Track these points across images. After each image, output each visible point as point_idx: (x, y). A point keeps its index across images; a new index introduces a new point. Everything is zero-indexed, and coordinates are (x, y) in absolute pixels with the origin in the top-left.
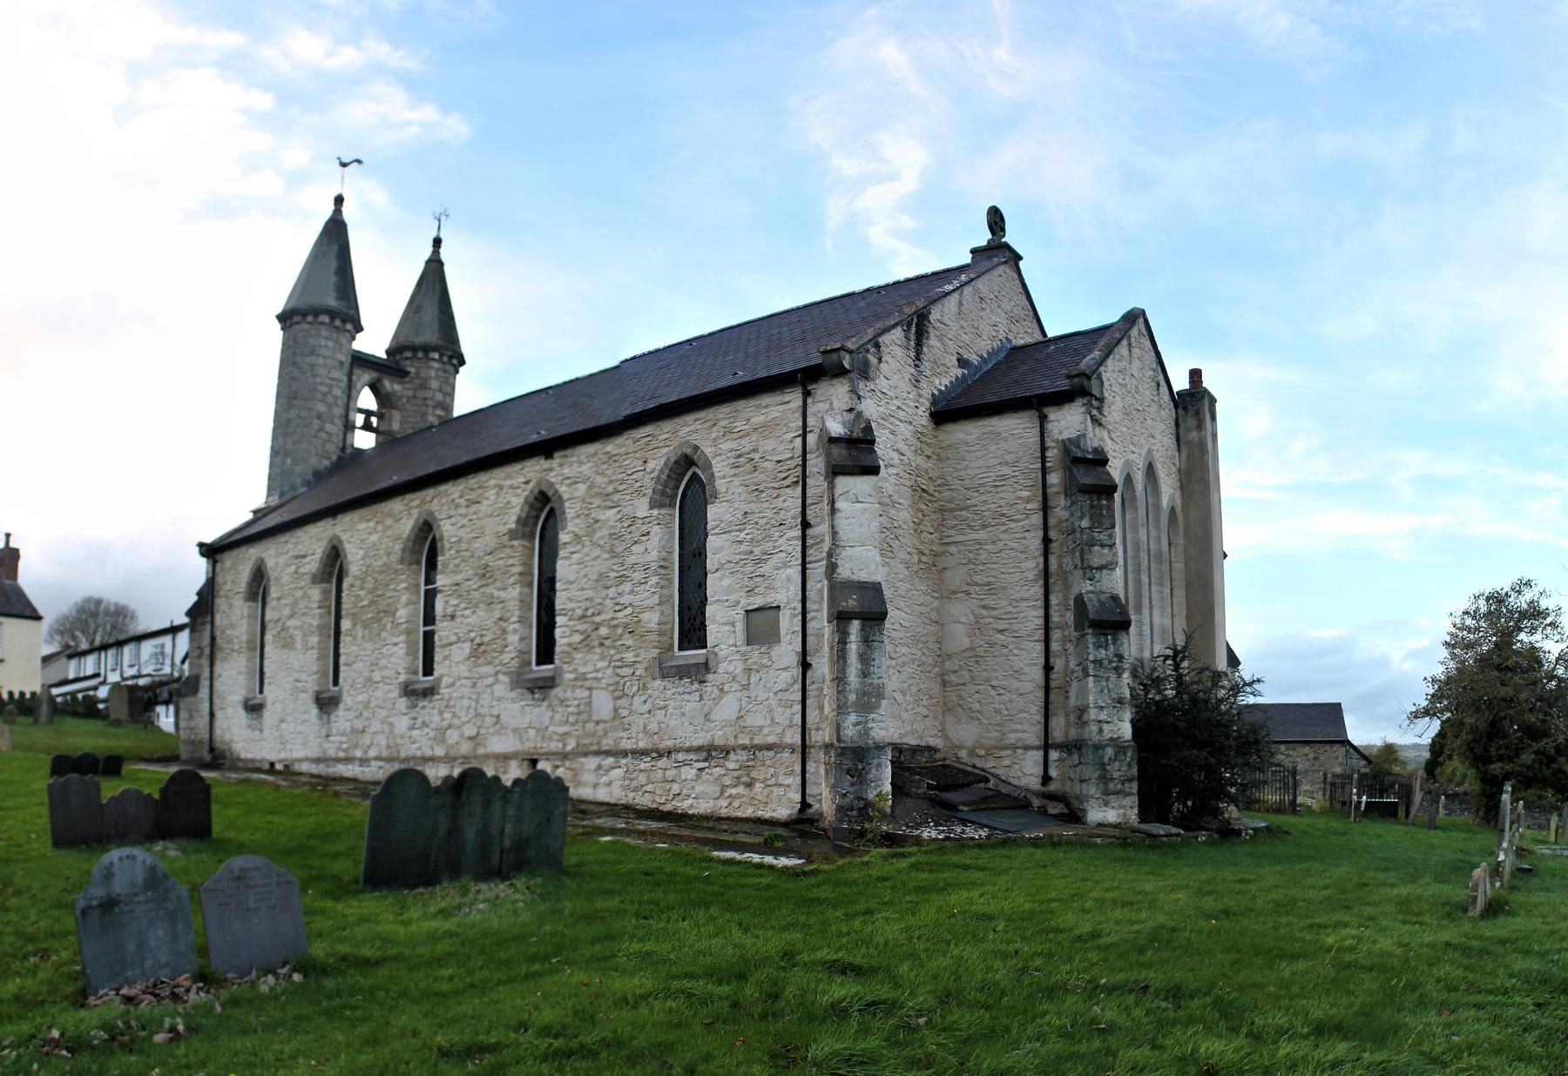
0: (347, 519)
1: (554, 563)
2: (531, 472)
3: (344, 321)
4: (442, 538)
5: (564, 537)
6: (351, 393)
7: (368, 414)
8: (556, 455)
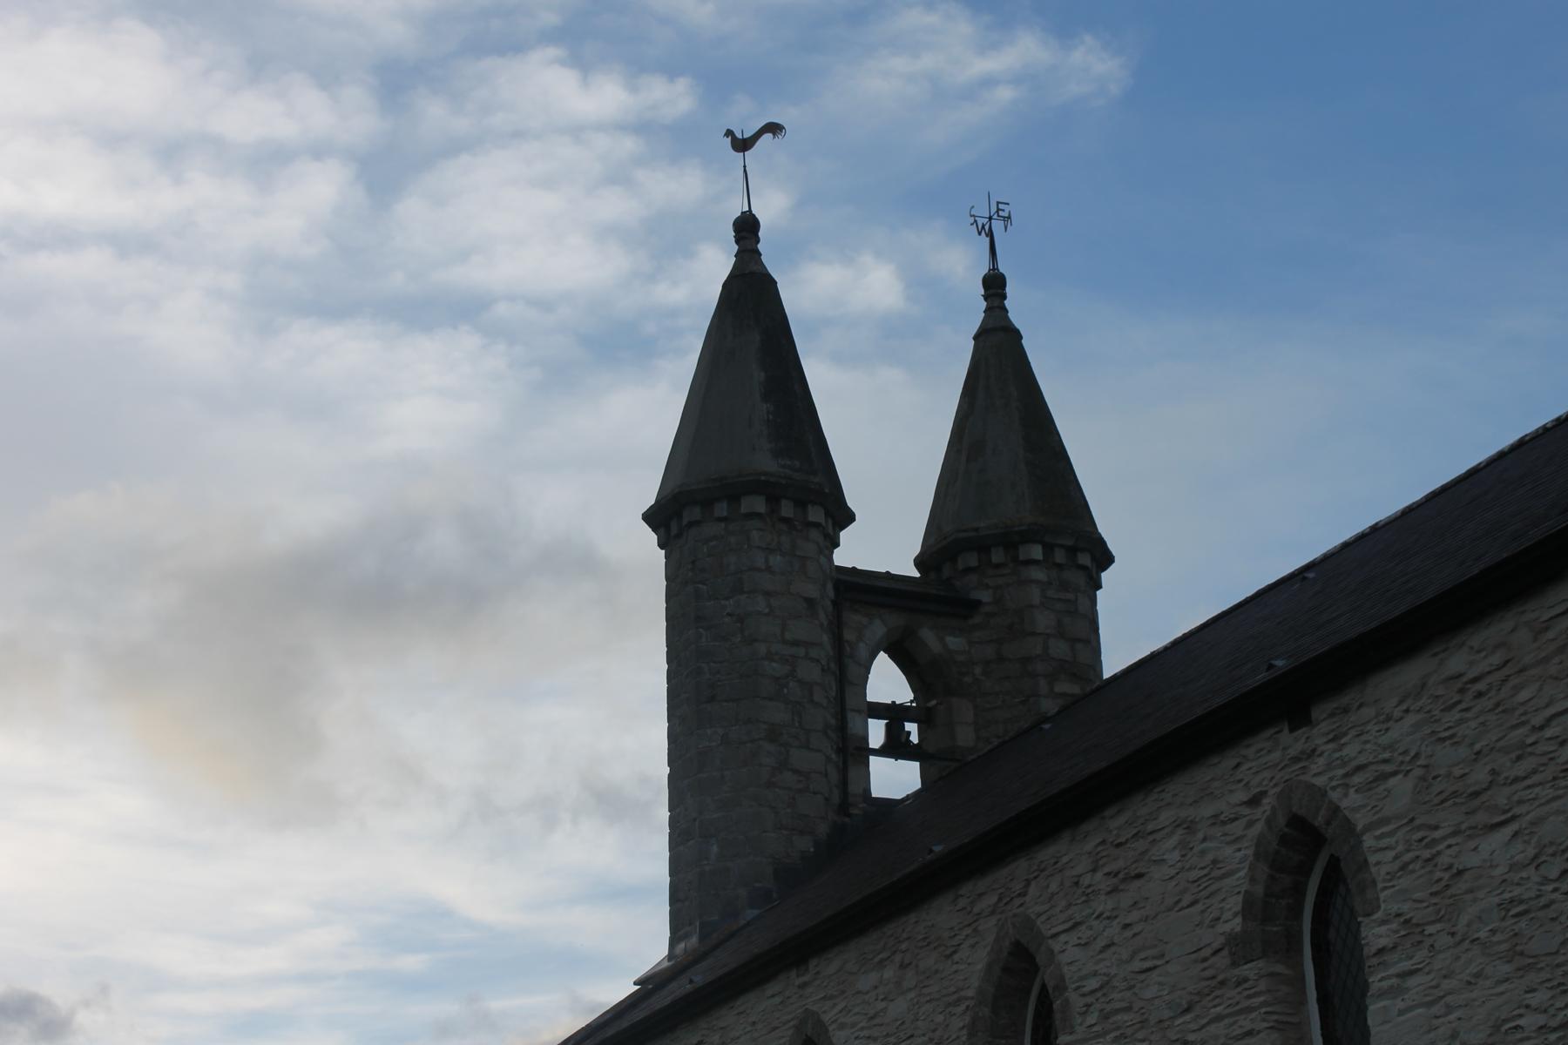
0: (831, 966)
1: (1362, 1010)
2: (1258, 771)
3: (801, 504)
4: (1061, 987)
5: (1376, 935)
6: (851, 676)
7: (893, 714)
8: (1318, 712)
